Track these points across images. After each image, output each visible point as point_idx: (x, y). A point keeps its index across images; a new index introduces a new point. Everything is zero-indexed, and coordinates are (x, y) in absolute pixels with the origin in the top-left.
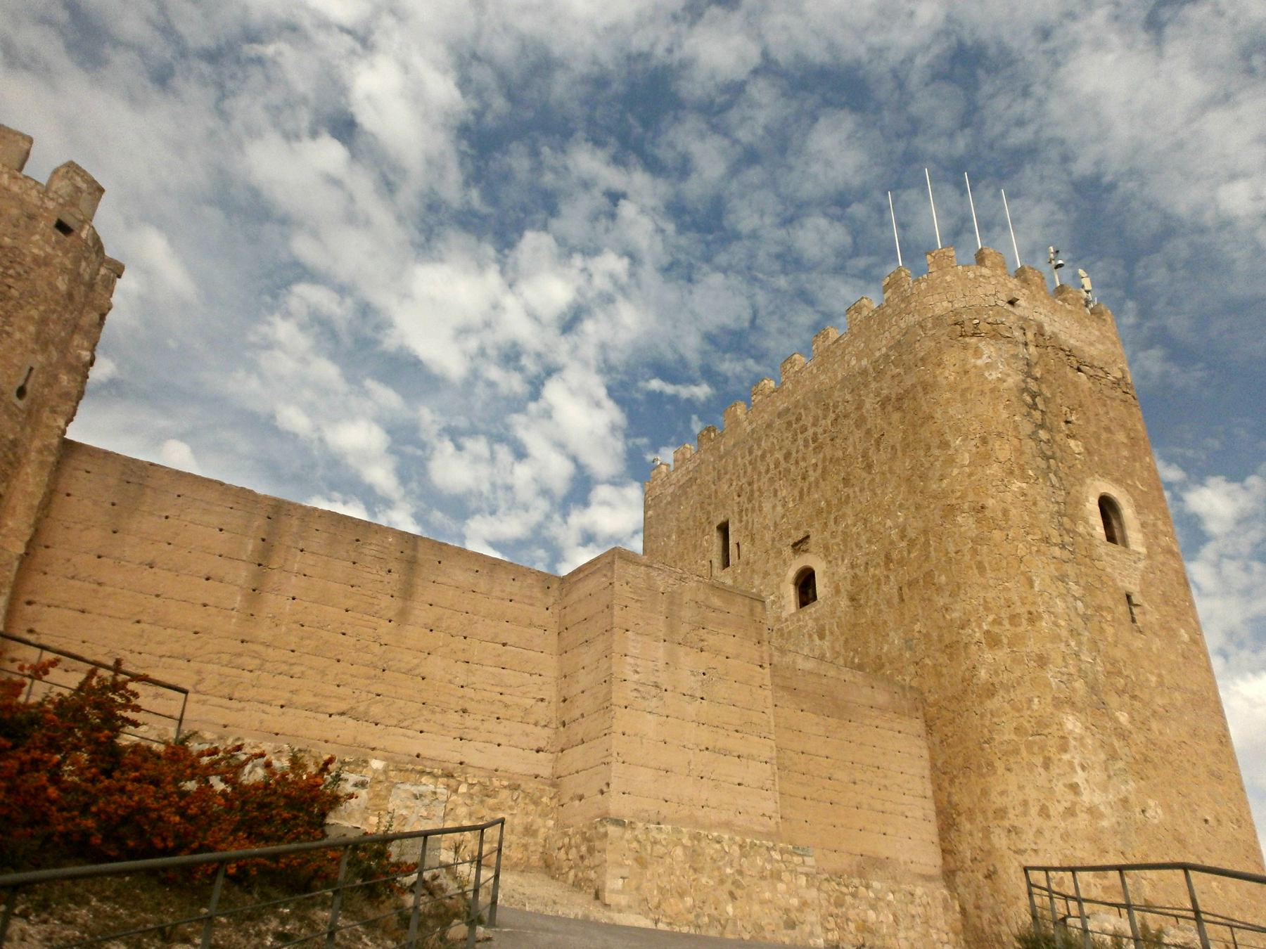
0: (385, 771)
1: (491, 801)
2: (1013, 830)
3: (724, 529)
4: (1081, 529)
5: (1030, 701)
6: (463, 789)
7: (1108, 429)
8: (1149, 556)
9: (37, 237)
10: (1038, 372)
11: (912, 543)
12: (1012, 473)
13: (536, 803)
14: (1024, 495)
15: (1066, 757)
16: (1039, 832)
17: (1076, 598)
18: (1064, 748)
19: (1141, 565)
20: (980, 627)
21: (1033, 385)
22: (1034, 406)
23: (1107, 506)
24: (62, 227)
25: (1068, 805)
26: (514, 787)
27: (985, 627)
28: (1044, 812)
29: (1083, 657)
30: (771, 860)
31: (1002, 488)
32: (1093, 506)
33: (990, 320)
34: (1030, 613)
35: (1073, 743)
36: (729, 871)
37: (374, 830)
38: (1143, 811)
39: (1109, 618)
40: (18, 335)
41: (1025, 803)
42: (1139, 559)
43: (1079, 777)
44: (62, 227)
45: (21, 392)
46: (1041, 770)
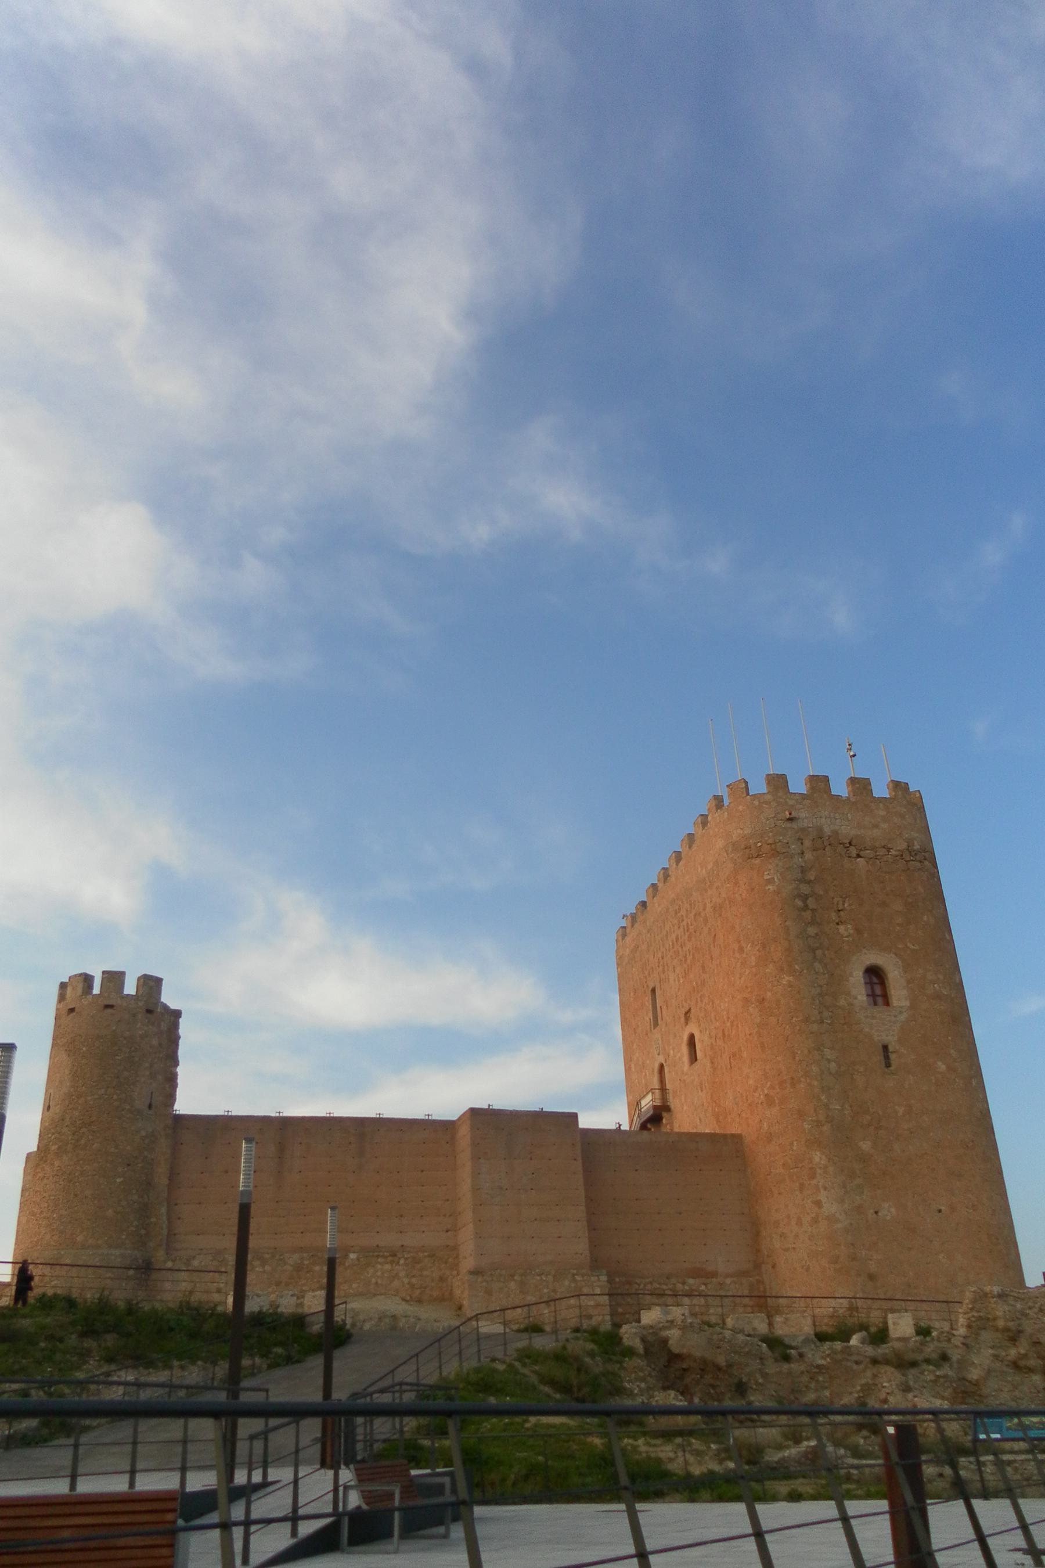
0: (358, 1259)
1: (418, 1266)
2: (783, 1235)
3: (653, 991)
4: (842, 1002)
5: (792, 1144)
6: (402, 1261)
7: (884, 904)
8: (913, 1007)
9: (139, 1025)
10: (811, 876)
11: (732, 1022)
12: (782, 970)
13: (446, 1263)
14: (791, 986)
15: (814, 1182)
16: (797, 1236)
17: (829, 1061)
18: (813, 1176)
19: (903, 1017)
20: (763, 1090)
21: (805, 889)
22: (806, 907)
23: (875, 974)
24: (149, 1011)
25: (813, 1215)
26: (431, 1256)
27: (766, 1091)
28: (799, 1223)
29: (831, 1107)
30: (575, 1281)
31: (775, 983)
32: (857, 978)
33: (770, 841)
34: (792, 1078)
35: (819, 1171)
36: (545, 1291)
37: (119, 1398)
38: (876, 1213)
39: (862, 1069)
40: (143, 1080)
41: (788, 1217)
42: (901, 1012)
43: (822, 1196)
44: (149, 1011)
45: (150, 1106)
46: (797, 1193)
